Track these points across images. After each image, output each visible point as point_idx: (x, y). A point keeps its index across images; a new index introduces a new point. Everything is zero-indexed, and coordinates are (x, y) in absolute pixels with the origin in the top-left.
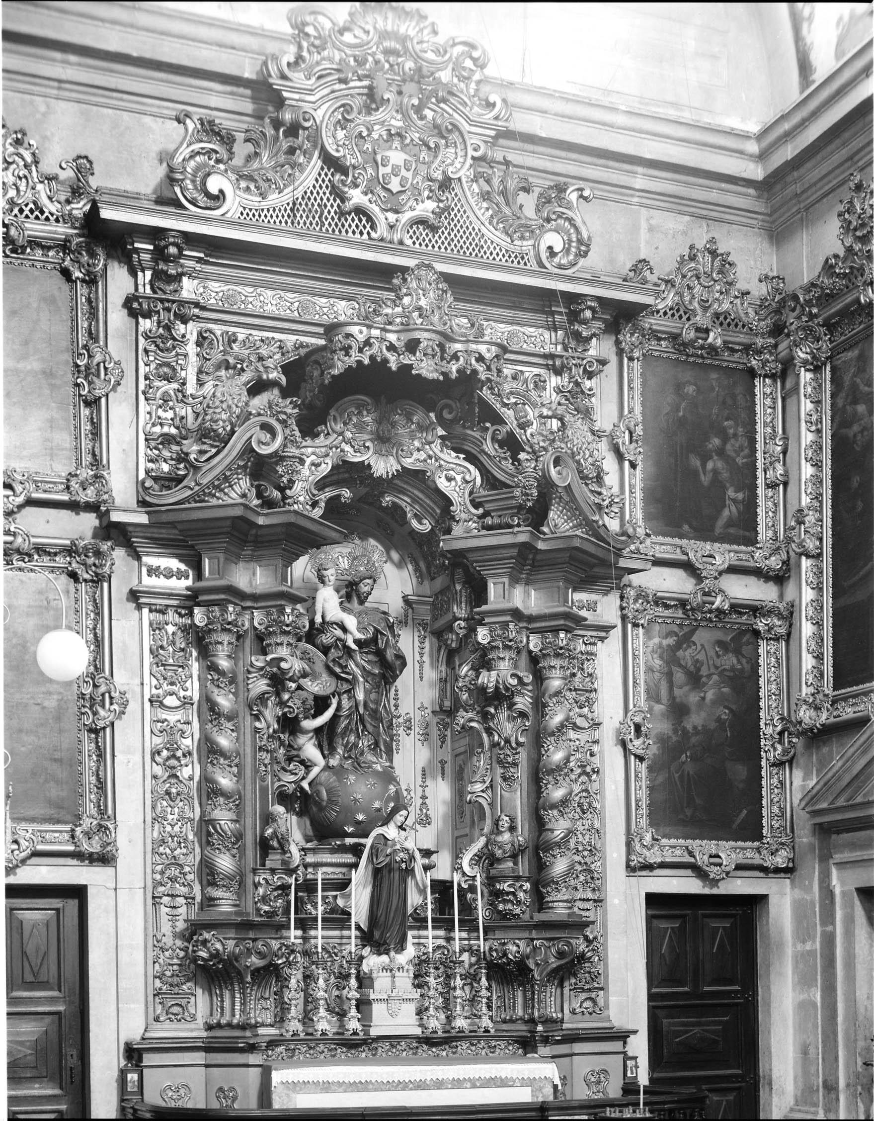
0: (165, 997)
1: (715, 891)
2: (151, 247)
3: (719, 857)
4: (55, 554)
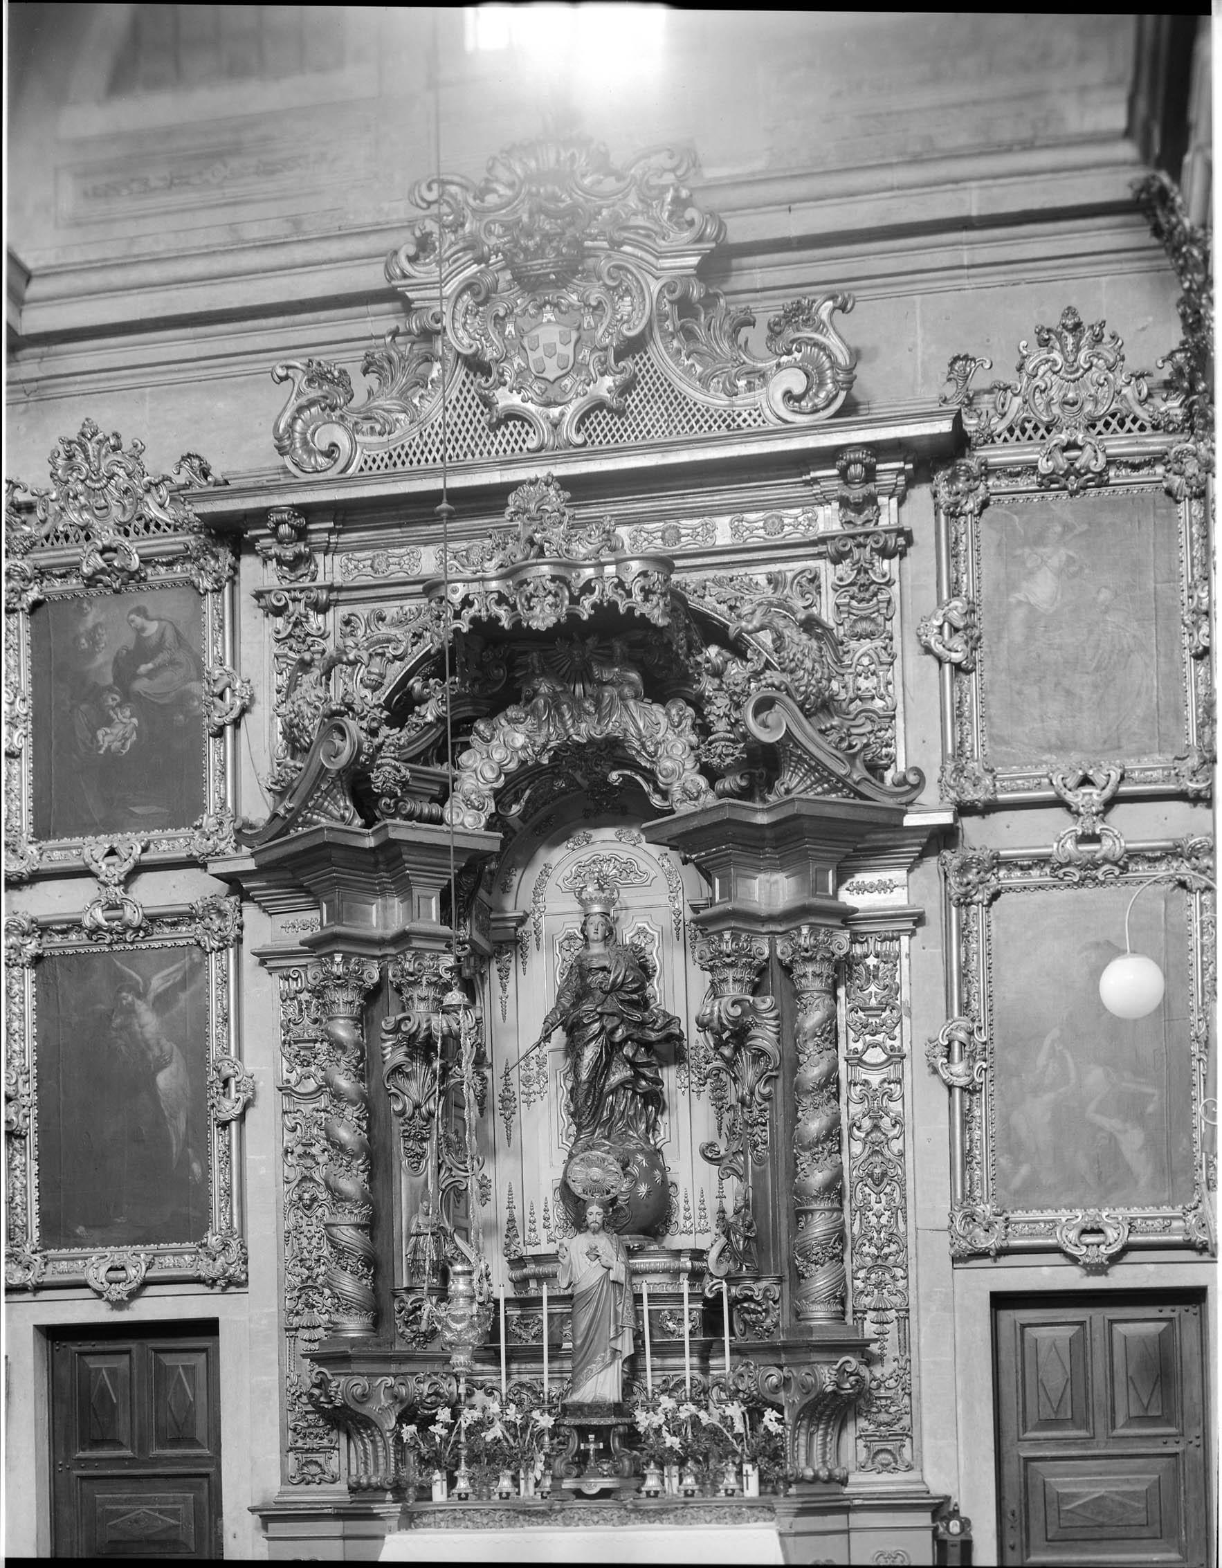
0: (302, 1454)
2: (835, 472)
4: (1030, 867)
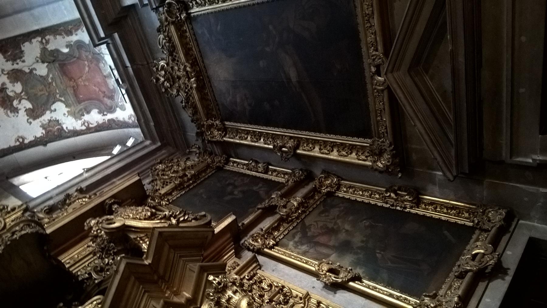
1: (511, 273)
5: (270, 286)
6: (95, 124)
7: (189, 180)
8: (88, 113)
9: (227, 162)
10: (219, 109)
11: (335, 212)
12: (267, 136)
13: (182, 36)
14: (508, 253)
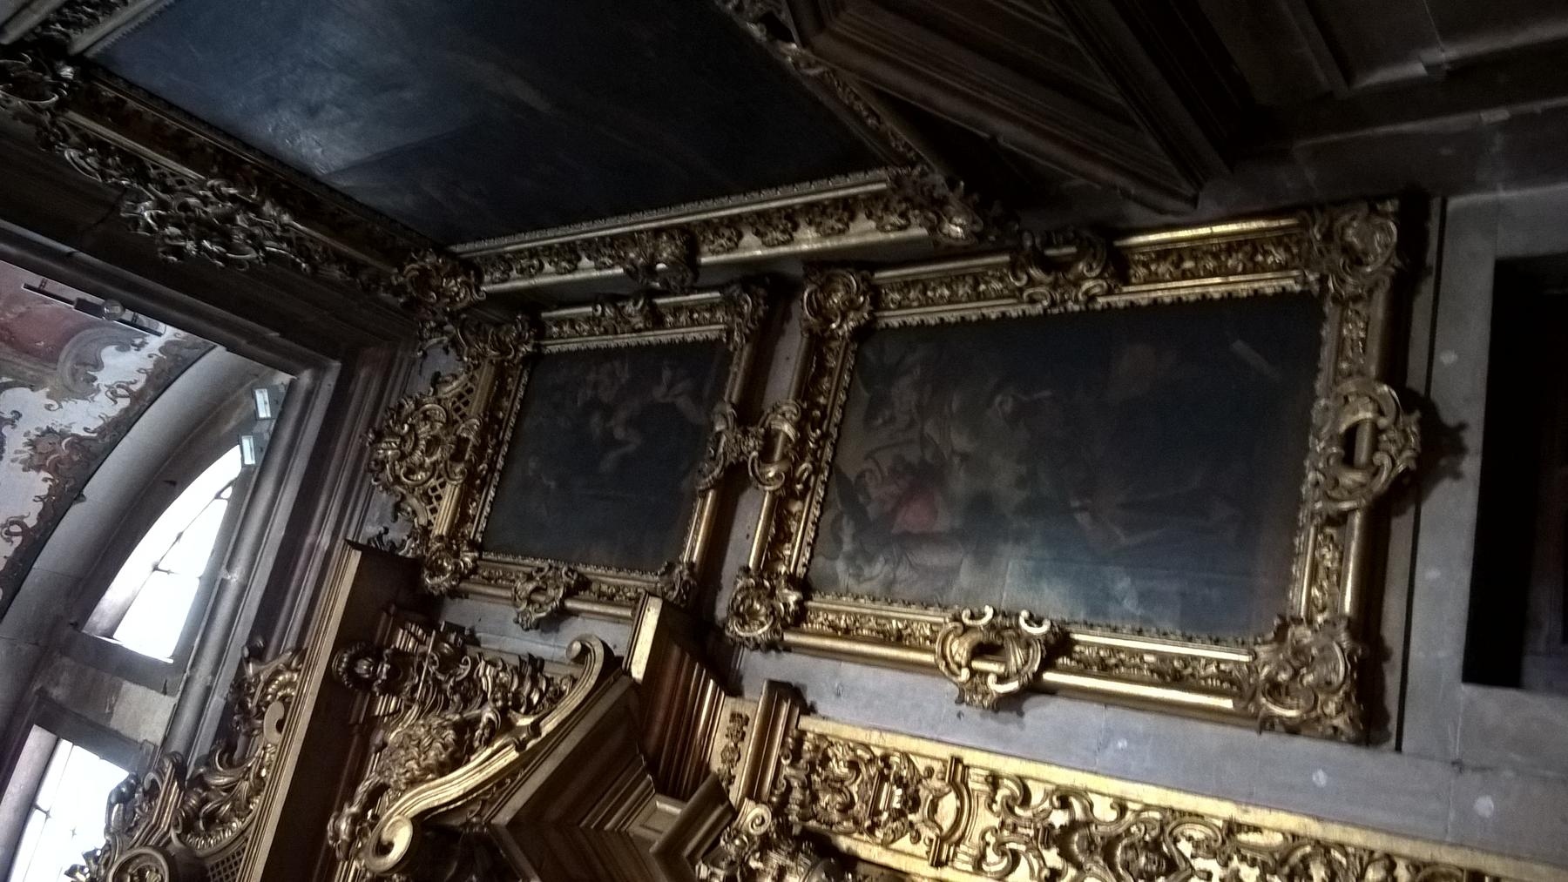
1: (1474, 439)
3: (1353, 431)
5: (853, 765)
6: (143, 378)
7: (480, 450)
8: (98, 365)
9: (541, 331)
10: (406, 228)
11: (904, 393)
12: (593, 248)
13: (123, 121)
14: (1446, 358)
